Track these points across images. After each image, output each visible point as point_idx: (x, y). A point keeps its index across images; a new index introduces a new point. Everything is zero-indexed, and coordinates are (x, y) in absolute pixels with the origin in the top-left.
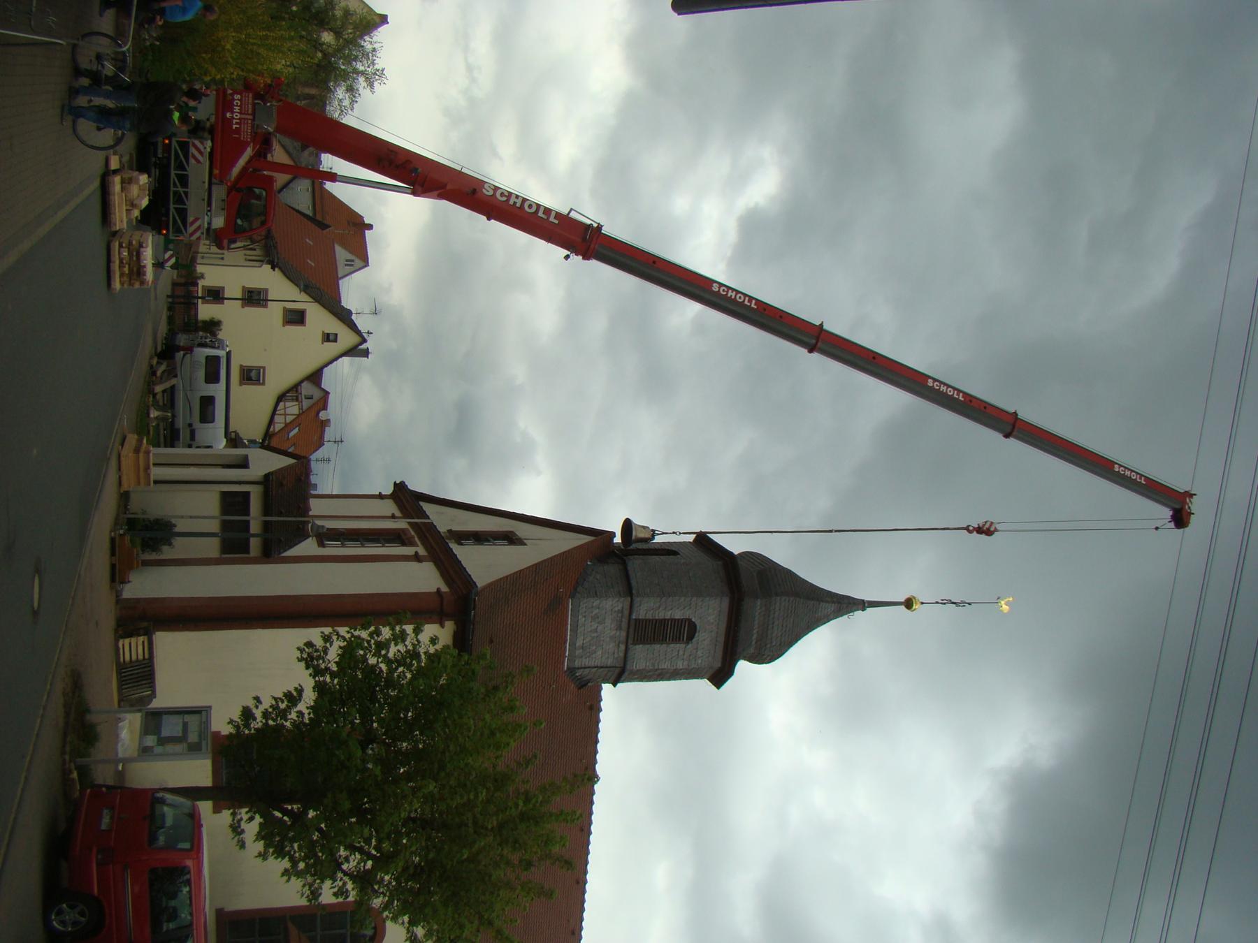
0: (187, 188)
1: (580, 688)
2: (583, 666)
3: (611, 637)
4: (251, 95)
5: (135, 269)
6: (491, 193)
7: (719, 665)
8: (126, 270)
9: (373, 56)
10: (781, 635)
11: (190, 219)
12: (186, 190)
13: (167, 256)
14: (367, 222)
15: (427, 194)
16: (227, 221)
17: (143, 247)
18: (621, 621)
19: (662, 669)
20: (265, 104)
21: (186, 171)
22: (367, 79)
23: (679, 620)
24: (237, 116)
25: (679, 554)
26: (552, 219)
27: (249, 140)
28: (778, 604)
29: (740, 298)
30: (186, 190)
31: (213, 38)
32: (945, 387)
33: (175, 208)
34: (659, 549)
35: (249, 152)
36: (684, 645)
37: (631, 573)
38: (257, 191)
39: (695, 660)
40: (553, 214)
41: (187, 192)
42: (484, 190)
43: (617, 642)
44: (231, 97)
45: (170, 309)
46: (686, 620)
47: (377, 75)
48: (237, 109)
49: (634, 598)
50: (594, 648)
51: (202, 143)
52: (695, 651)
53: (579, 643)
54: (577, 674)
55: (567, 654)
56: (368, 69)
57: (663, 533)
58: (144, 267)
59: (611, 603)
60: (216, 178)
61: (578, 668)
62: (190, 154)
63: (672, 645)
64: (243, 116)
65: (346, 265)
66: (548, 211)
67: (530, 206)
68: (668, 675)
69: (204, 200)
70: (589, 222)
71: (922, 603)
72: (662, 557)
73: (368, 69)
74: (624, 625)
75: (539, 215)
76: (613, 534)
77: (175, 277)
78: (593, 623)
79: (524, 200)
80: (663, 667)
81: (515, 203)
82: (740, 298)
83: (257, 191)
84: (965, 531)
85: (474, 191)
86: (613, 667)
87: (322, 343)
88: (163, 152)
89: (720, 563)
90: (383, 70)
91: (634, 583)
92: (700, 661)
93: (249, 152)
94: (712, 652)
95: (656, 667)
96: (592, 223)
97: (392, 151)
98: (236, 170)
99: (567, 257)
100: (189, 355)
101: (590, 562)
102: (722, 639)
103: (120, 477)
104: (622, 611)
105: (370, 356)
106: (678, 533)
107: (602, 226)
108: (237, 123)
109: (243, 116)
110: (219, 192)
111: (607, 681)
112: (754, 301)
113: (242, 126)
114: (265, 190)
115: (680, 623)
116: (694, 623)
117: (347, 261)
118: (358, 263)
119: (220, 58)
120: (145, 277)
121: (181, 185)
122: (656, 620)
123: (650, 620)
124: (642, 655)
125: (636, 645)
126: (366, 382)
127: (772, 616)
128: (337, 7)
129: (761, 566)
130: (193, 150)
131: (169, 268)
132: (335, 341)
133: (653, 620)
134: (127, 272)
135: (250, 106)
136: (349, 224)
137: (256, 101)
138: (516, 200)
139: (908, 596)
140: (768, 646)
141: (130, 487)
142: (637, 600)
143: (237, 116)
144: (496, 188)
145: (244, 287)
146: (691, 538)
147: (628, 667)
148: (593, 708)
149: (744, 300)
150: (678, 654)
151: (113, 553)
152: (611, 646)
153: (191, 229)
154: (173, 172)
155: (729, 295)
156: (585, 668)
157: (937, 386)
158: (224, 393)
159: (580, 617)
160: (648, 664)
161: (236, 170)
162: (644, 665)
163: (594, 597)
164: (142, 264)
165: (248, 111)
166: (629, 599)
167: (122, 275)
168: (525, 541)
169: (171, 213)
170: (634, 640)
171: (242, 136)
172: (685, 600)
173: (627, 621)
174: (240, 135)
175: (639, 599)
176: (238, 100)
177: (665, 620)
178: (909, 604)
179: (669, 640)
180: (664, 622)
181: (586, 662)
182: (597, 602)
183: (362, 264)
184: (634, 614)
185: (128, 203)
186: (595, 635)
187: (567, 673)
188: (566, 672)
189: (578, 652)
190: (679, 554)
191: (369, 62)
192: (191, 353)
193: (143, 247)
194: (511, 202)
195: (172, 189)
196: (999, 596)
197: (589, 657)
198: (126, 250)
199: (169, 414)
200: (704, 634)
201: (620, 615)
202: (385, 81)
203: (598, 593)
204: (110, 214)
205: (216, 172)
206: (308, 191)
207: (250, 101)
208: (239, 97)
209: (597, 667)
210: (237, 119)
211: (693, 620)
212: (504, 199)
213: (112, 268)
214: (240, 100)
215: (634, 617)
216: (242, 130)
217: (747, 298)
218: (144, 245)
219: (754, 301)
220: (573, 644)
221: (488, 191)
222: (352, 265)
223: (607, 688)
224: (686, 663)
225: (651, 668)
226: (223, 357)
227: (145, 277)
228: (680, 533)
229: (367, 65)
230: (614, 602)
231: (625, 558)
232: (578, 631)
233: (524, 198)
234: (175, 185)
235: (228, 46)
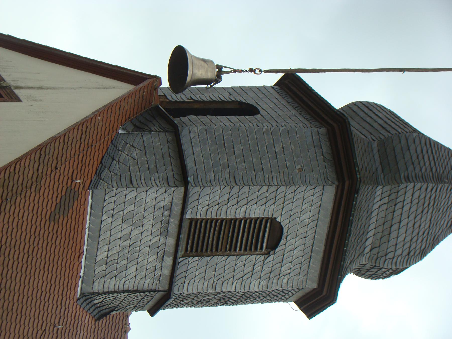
2: (106, 290)
7: (315, 285)
23: (256, 220)
25: (257, 112)
28: (409, 194)
34: (227, 102)
37: (186, 147)
49: (190, 188)
50: (125, 262)
53: (101, 256)
54: (96, 302)
57: (235, 71)
59: (154, 196)
61: (98, 294)
63: (244, 257)
72: (234, 119)
76: (157, 79)
78: (124, 226)
80: (229, 290)
86: (152, 291)
91: (189, 163)
94: (305, 267)
95: (218, 290)
101: (123, 129)
106: (257, 71)
111: (138, 308)
122: (222, 221)
125: (189, 257)
127: (398, 213)
129: (383, 131)
133: (217, 220)
140: (390, 256)
142: (194, 191)
147: (175, 290)
152: (150, 260)
159: (105, 217)
166: (182, 189)
168: (17, 92)
170: (186, 250)
173: (177, 222)
175: (197, 189)
177: (236, 220)
179: (240, 250)
181: (111, 285)
184: (189, 212)
186: (127, 243)
187: (79, 302)
188: (78, 299)
190: (257, 112)
201: (167, 213)
209: (128, 291)
211: (279, 220)
224: (264, 283)
225: (210, 291)
228: (261, 71)
231: (176, 121)
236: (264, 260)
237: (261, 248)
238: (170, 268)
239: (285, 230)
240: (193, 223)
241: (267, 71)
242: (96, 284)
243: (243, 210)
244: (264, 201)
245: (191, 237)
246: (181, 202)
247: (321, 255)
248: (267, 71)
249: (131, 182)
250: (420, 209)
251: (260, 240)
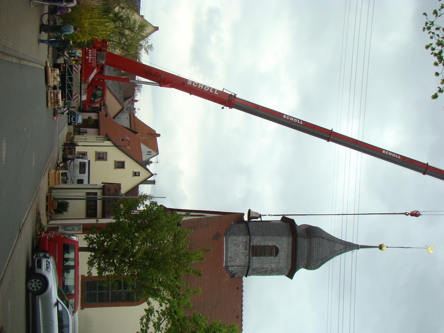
0: (72, 82)
1: (231, 278)
3: (243, 253)
4: (95, 50)
5: (56, 101)
6: (191, 84)
8: (53, 101)
9: (147, 39)
10: (318, 255)
11: (74, 94)
12: (72, 83)
13: (65, 110)
14: (157, 133)
15: (165, 86)
16: (88, 97)
17: (58, 93)
18: (246, 246)
19: (266, 268)
20: (101, 53)
21: (72, 76)
22: (145, 49)
23: (271, 246)
24: (90, 58)
26: (215, 93)
27: (95, 66)
29: (295, 120)
30: (72, 83)
31: (81, 23)
32: (391, 153)
33: (68, 90)
35: (95, 71)
36: (274, 257)
38: (99, 87)
39: (279, 264)
40: (216, 91)
41: (72, 84)
42: (188, 83)
43: (245, 256)
44: (88, 51)
45: (63, 151)
46: (274, 246)
47: (149, 47)
48: (90, 55)
51: (78, 66)
52: (279, 260)
53: (229, 255)
55: (224, 260)
56: (145, 45)
58: (59, 100)
60: (83, 81)
62: (73, 70)
63: (269, 257)
64: (92, 58)
65: (148, 154)
66: (214, 90)
67: (207, 88)
68: (269, 272)
69: (79, 86)
70: (230, 93)
71: (387, 247)
73: (145, 45)
74: (248, 248)
75: (210, 91)
77: (65, 141)
78: (234, 247)
79: (204, 86)
80: (266, 267)
81: (200, 87)
82: (295, 120)
83: (99, 87)
84: (405, 215)
85: (184, 83)
87: (133, 177)
88: (63, 69)
89: (288, 224)
90: (152, 45)
91: (251, 230)
92: (281, 265)
93: (95, 71)
95: (263, 267)
96: (232, 93)
97: (150, 69)
98: (91, 78)
99: (223, 108)
100: (72, 162)
101: (233, 222)
102: (290, 255)
103: (49, 181)
104: (246, 242)
105: (156, 183)
107: (236, 95)
108: (90, 60)
109: (92, 58)
110: (84, 86)
112: (301, 121)
113: (93, 61)
114: (102, 87)
115: (271, 247)
116: (277, 247)
117: (148, 152)
118: (153, 153)
119: (83, 30)
120: (59, 103)
121: (70, 81)
123: (258, 246)
124: (256, 262)
126: (113, 69)
128: (131, 20)
130: (74, 68)
131: (66, 114)
132: (139, 175)
134: (53, 102)
135: (95, 54)
136: (148, 134)
137: (98, 52)
138: (201, 86)
139: (380, 244)
141: (52, 185)
143: (90, 58)
144: (193, 82)
145: (96, 152)
146: (279, 218)
148: (239, 289)
149: (297, 121)
150: (272, 261)
151: (47, 201)
153: (74, 98)
154: (67, 76)
155: (291, 119)
156: (232, 266)
157: (387, 153)
158: (87, 178)
159: (229, 244)
160: (259, 265)
161: (91, 78)
162: (257, 265)
163: (234, 236)
164: (58, 99)
165: (94, 56)
166: (249, 236)
167: (51, 103)
169: (66, 92)
171: (93, 65)
172: (273, 237)
173: (249, 246)
174: (92, 65)
176: (90, 52)
178: (381, 247)
179: (267, 255)
180: (264, 247)
181: (233, 264)
182: (235, 238)
183: (155, 153)
184: (252, 243)
185: (53, 78)
186: (236, 252)
189: (229, 259)
191: (146, 42)
192: (73, 161)
193: (58, 93)
194: (199, 87)
195: (67, 83)
196: (426, 245)
197: (234, 261)
198: (53, 94)
199: (65, 178)
200: (282, 253)
201: (245, 243)
202: (153, 49)
203: (236, 234)
204: (48, 79)
205: (83, 78)
206: (128, 119)
207: (95, 52)
208: (91, 50)
210: (90, 59)
211: (277, 246)
212: (196, 86)
213: (48, 99)
214: (92, 52)
215: (252, 245)
216: (93, 63)
217: (298, 120)
218: (59, 93)
219: (301, 121)
220: (227, 256)
221: (190, 83)
222: (150, 154)
223: (244, 278)
224: (275, 265)
226: (87, 162)
227: (59, 103)
229: (145, 43)
230: (243, 238)
232: (229, 250)
233: (204, 85)
234: (68, 81)
235: (86, 25)
236: (275, 258)
237: (273, 255)
238: (248, 259)
239: (279, 250)
240: (253, 247)
241: (274, 215)
242: (229, 263)
243: (266, 243)
244: (272, 240)
245: (253, 251)
246: (249, 240)
247: (291, 257)
248: (274, 215)
249: (235, 235)
250: (319, 246)
251: (273, 252)
